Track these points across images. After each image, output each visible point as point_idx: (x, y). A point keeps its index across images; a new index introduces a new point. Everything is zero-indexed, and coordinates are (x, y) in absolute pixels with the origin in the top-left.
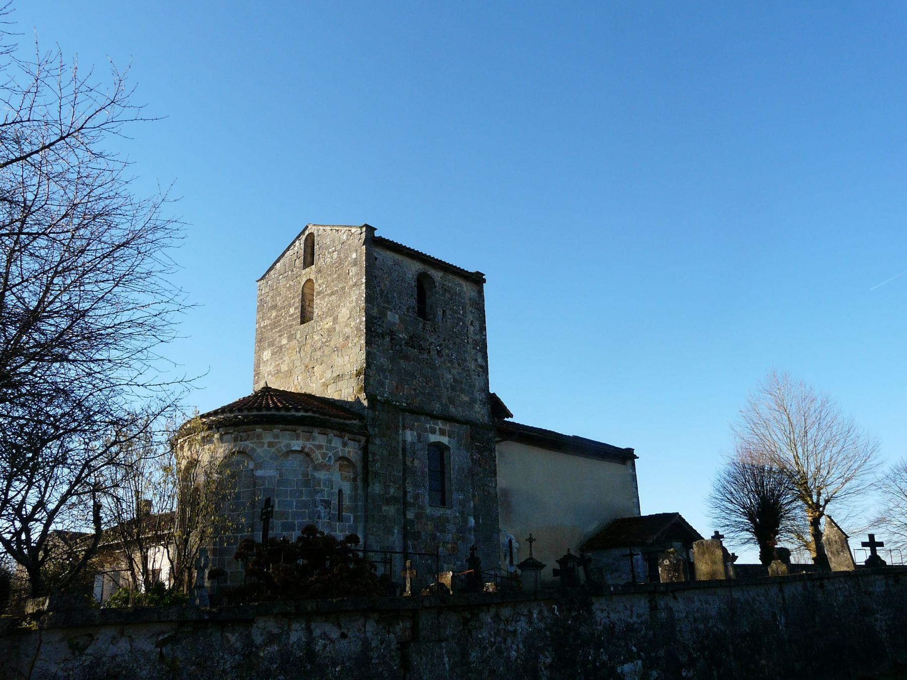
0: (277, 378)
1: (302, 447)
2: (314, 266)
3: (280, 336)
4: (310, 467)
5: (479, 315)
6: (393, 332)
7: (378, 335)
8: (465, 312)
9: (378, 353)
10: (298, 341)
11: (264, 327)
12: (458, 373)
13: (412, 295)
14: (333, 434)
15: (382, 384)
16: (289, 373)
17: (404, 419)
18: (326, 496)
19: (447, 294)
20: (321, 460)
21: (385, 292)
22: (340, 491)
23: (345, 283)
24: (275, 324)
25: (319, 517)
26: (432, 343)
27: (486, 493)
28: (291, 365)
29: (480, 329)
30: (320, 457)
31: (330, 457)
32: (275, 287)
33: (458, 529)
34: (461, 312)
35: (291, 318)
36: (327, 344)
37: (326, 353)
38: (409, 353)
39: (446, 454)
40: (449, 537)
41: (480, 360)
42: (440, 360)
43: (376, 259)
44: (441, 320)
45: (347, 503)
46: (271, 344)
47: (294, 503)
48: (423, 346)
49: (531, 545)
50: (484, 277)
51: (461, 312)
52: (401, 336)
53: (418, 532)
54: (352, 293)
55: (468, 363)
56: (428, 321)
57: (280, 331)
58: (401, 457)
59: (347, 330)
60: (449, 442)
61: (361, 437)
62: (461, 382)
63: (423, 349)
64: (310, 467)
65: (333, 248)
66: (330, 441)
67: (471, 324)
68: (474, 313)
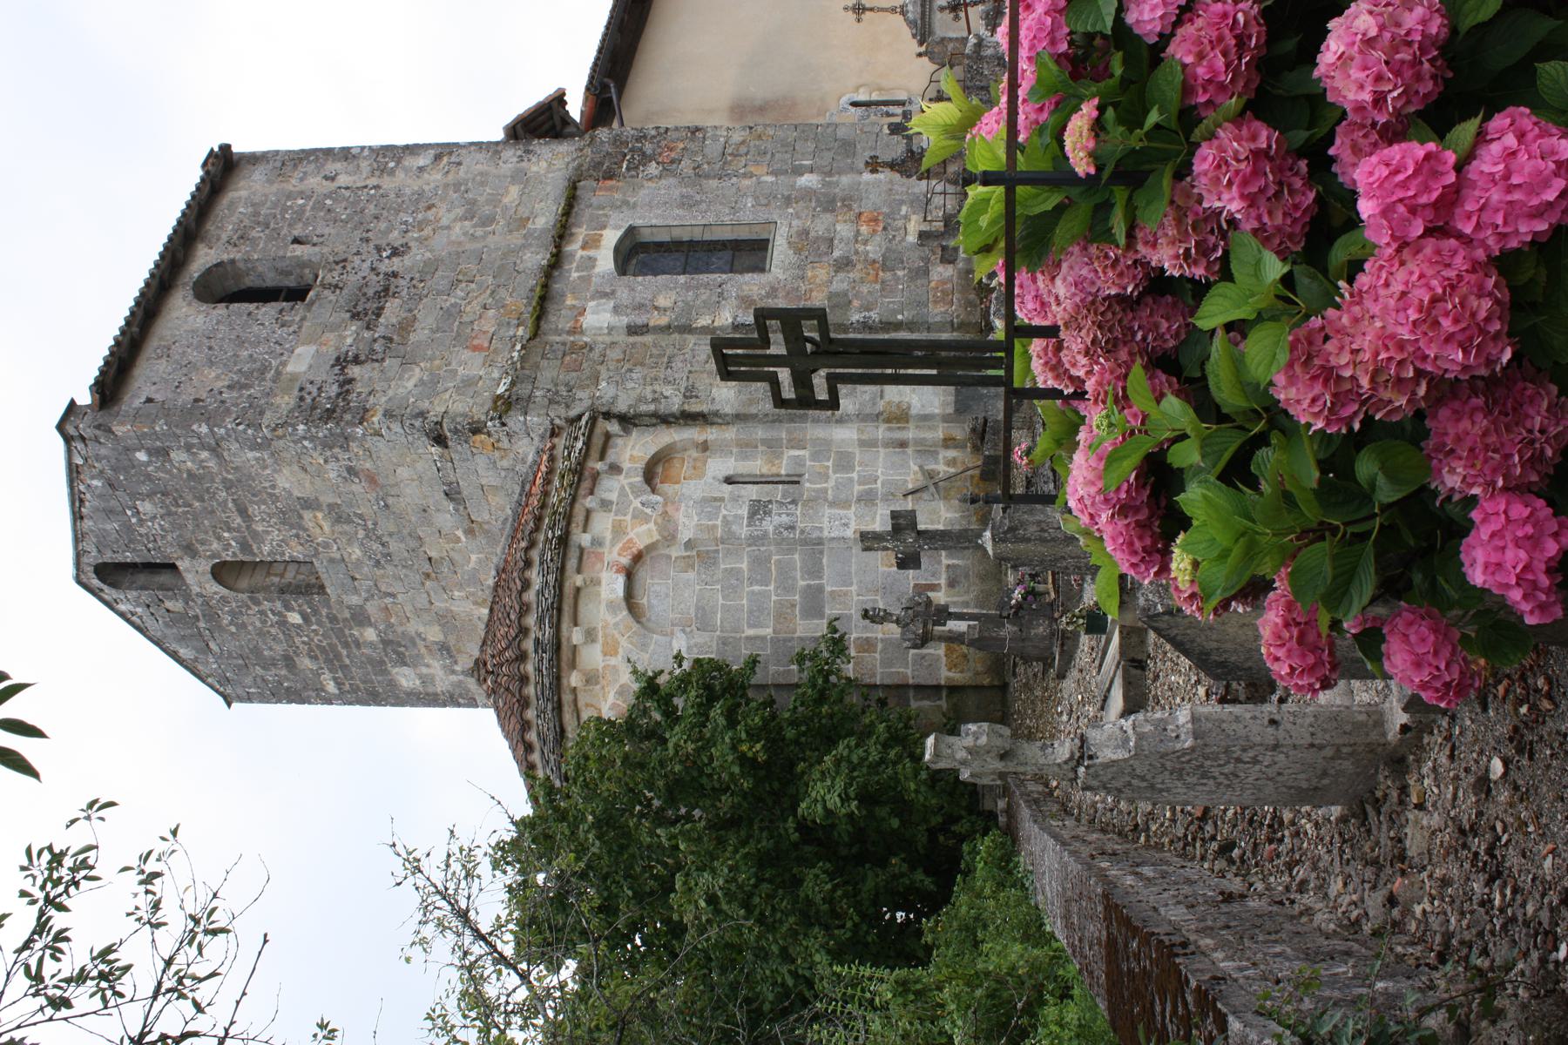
0: (459, 651)
1: (618, 571)
2: (178, 563)
3: (358, 645)
4: (667, 551)
5: (310, 162)
6: (338, 359)
7: (344, 394)
8: (301, 194)
9: (390, 393)
10: (366, 600)
11: (339, 684)
12: (449, 211)
13: (249, 314)
14: (585, 496)
15: (469, 382)
16: (446, 620)
17: (558, 332)
18: (740, 512)
19: (254, 234)
20: (652, 525)
21: (236, 378)
22: (729, 481)
23: (213, 481)
24: (331, 659)
25: (791, 528)
26: (373, 269)
27: (743, 150)
28: (426, 617)
29: (346, 159)
30: (645, 527)
31: (643, 504)
32: (241, 662)
33: (826, 210)
34: (301, 202)
35: (313, 619)
36: (370, 523)
37: (392, 528)
38: (394, 321)
39: (647, 236)
40: (844, 230)
41: (422, 161)
42: (414, 250)
43: (149, 400)
44: (317, 249)
45: (757, 465)
46: (379, 666)
47: (756, 588)
48: (380, 289)
49: (871, 9)
50: (216, 149)
51: (301, 202)
52: (349, 341)
53: (829, 299)
54: (238, 461)
55: (426, 188)
56: (317, 277)
57: (346, 645)
58: (648, 339)
59: (332, 472)
60: (617, 227)
61: (598, 431)
62: (474, 202)
63: (386, 289)
64: (667, 551)
65: (129, 513)
66: (606, 505)
67: (333, 179)
68: (305, 173)
